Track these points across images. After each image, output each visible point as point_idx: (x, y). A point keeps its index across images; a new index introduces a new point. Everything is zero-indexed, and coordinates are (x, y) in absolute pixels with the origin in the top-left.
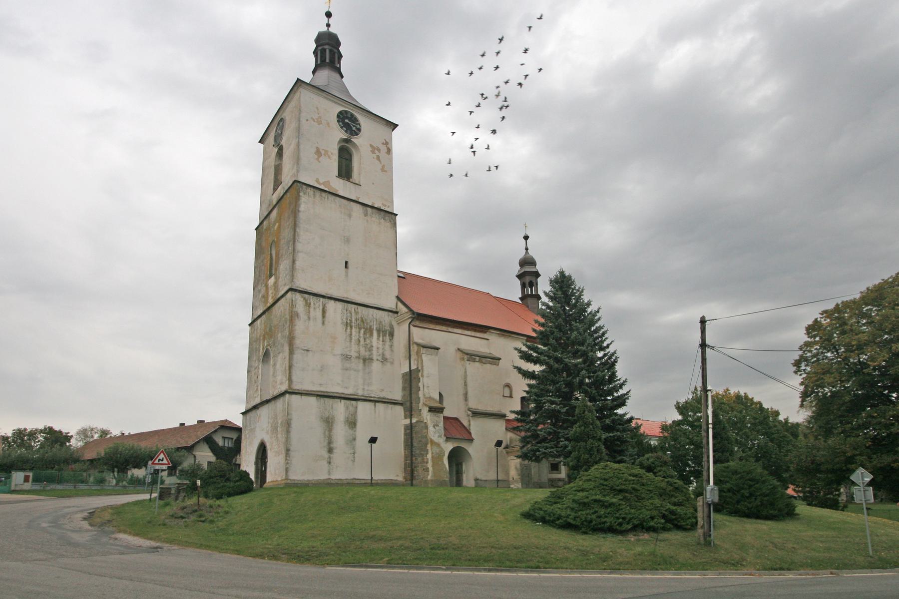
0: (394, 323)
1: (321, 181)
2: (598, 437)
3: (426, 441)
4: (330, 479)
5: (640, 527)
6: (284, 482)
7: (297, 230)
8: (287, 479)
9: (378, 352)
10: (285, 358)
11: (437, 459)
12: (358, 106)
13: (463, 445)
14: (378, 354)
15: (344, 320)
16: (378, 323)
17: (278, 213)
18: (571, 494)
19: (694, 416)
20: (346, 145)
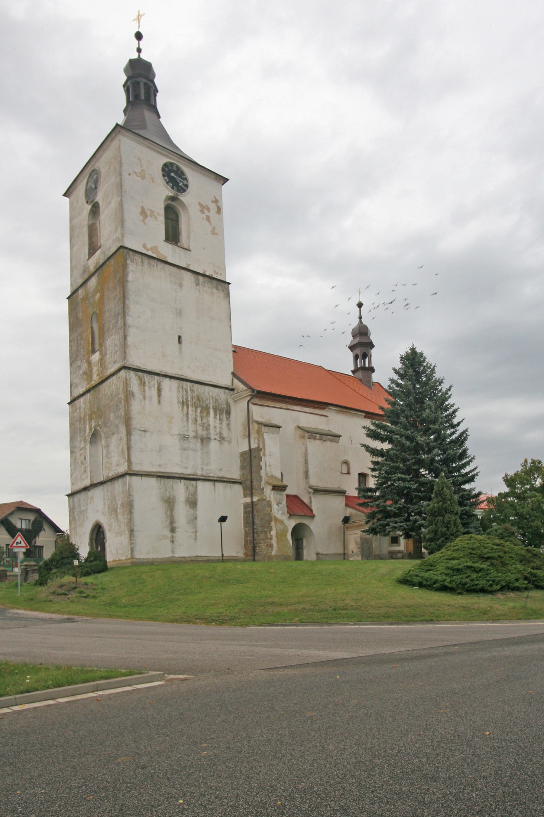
0: (231, 401)
1: (149, 246)
2: (455, 512)
3: (269, 519)
4: (173, 557)
5: (507, 587)
6: (129, 561)
7: (127, 302)
8: (132, 557)
9: (215, 431)
10: (121, 440)
11: (281, 535)
12: (183, 155)
13: (306, 521)
14: (216, 433)
15: (180, 398)
16: (214, 401)
17: (98, 283)
18: (442, 562)
19: (521, 488)
20: (173, 203)
